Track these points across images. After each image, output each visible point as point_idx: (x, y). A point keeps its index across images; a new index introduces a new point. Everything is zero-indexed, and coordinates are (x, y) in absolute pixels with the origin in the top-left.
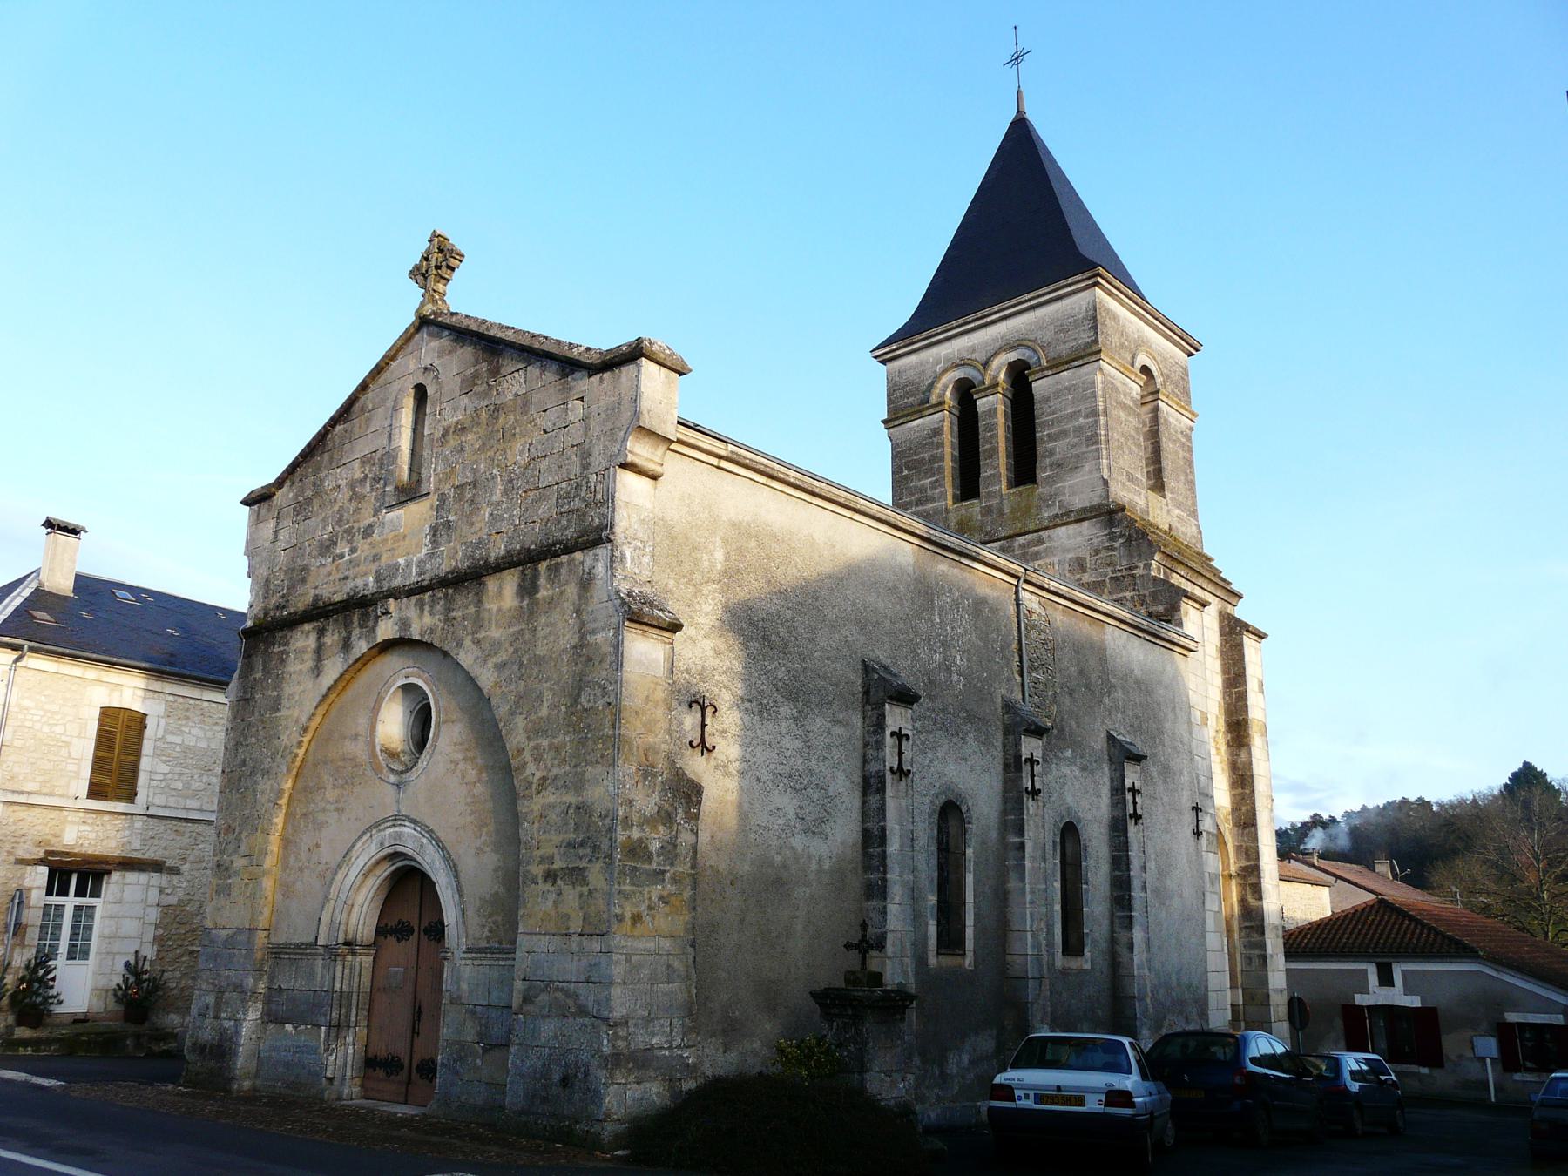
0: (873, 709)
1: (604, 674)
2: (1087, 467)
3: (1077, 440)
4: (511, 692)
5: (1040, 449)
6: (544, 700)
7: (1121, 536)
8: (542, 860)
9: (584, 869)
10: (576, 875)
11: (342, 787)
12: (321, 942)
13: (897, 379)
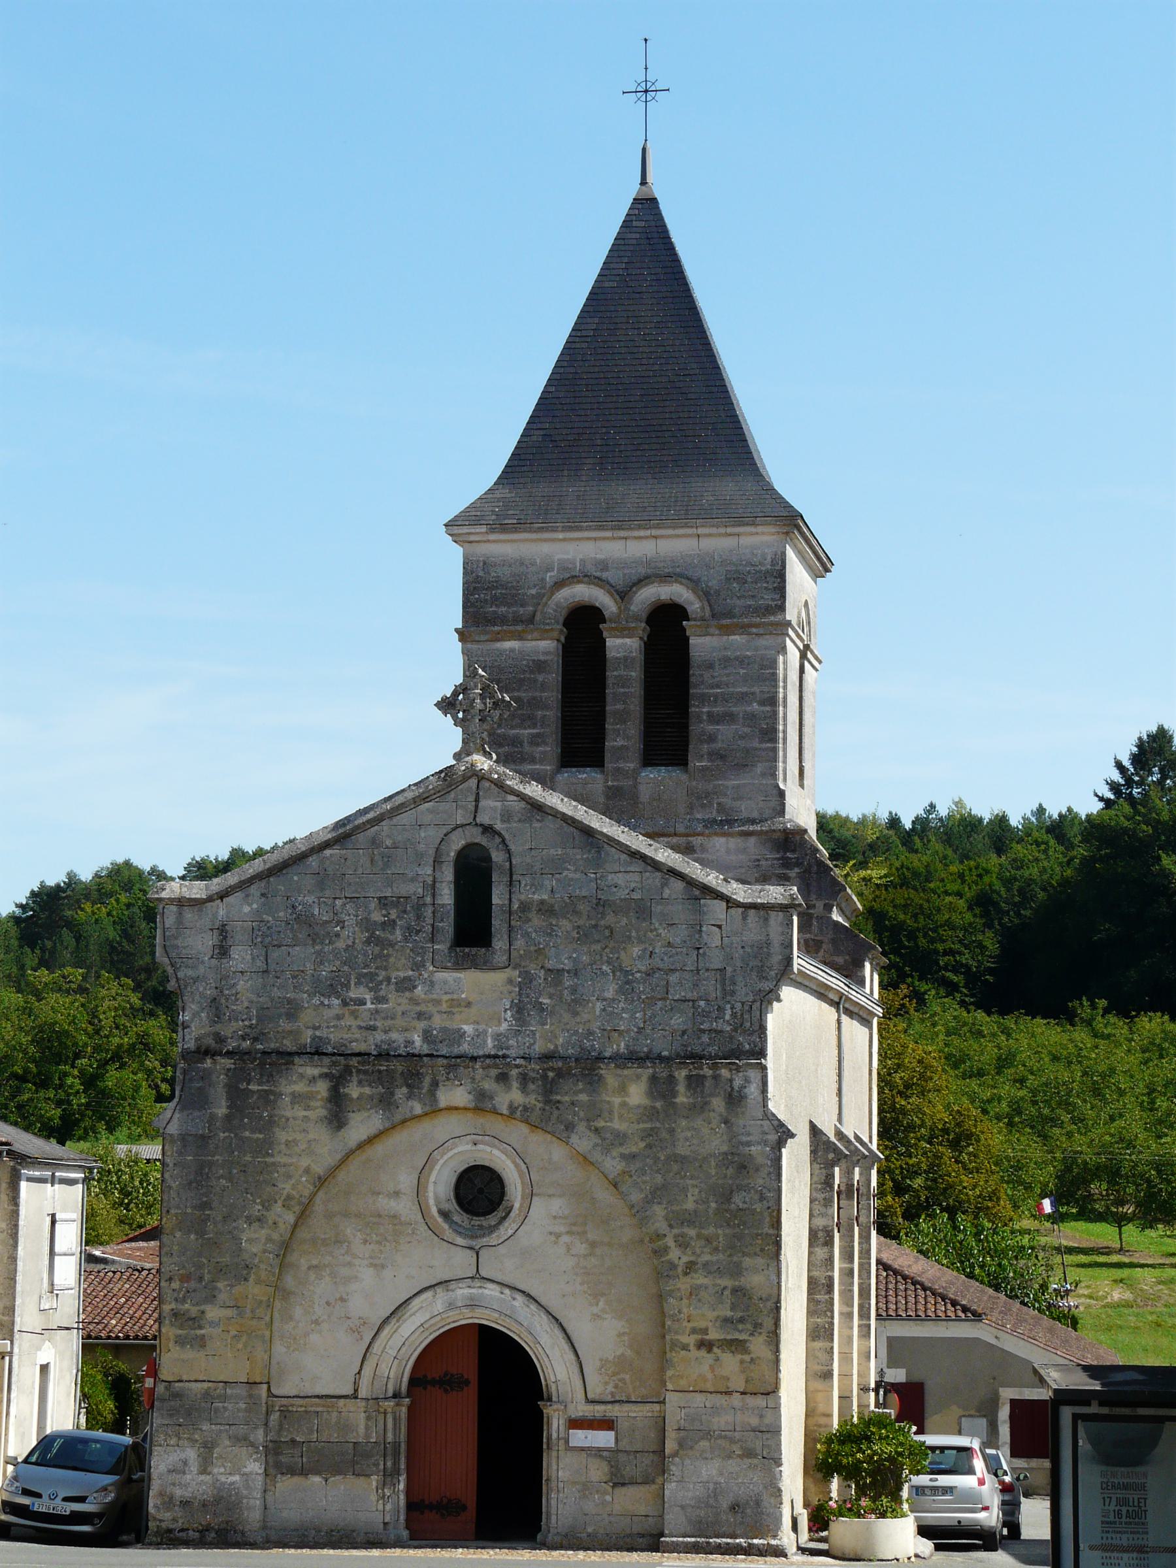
0: (821, 1168)
1: (761, 1182)
2: (759, 768)
3: (747, 730)
4: (645, 1182)
5: (695, 729)
6: (689, 1195)
7: (798, 864)
8: (694, 1331)
9: (745, 1341)
10: (736, 1346)
11: (379, 1243)
12: (363, 1393)
13: (481, 574)
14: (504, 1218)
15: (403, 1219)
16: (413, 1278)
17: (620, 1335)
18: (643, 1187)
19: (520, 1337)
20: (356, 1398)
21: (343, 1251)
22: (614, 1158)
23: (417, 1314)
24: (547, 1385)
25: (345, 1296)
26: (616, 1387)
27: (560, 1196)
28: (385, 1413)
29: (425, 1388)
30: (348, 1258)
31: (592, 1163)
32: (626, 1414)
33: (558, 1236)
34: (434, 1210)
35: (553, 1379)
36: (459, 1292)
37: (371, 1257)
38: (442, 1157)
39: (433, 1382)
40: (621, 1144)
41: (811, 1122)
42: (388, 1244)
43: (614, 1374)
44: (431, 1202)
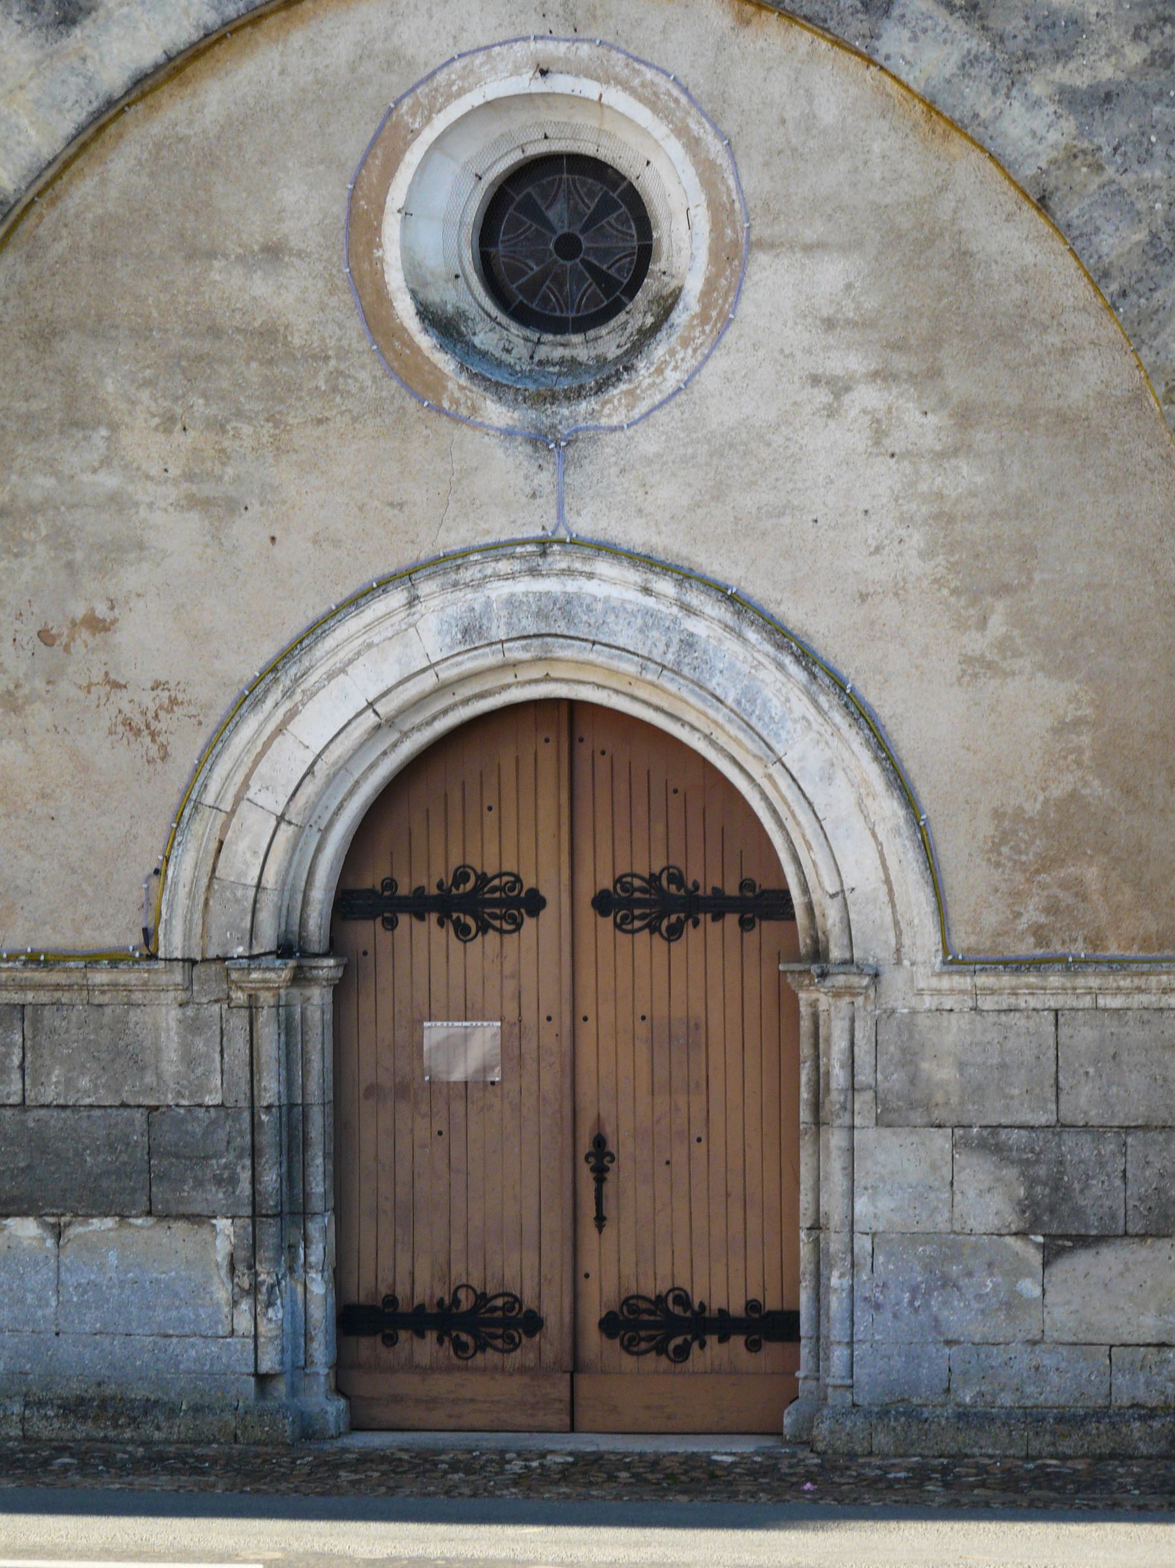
4: (1146, 188)
12: (173, 942)
14: (647, 335)
15: (297, 341)
16: (337, 543)
17: (1061, 729)
18: (1141, 205)
19: (713, 743)
20: (153, 957)
21: (94, 458)
22: (1037, 104)
23: (353, 670)
24: (810, 908)
25: (101, 610)
26: (1052, 909)
27: (845, 249)
28: (252, 1007)
29: (391, 924)
30: (109, 481)
31: (956, 126)
32: (1087, 1002)
33: (840, 387)
34: (405, 310)
35: (831, 887)
36: (499, 591)
37: (189, 477)
38: (428, 120)
39: (419, 905)
40: (1062, 56)
41: (600, 1231)
42: (247, 430)
43: (1047, 863)
44: (395, 280)
